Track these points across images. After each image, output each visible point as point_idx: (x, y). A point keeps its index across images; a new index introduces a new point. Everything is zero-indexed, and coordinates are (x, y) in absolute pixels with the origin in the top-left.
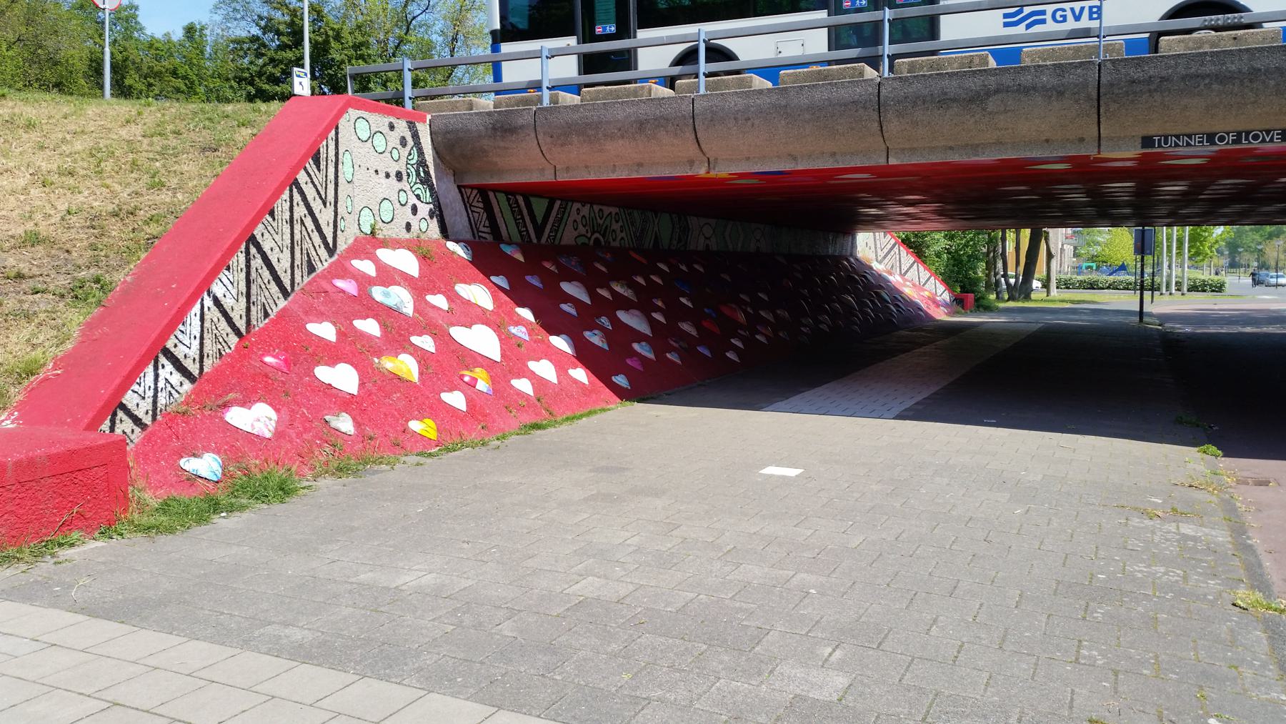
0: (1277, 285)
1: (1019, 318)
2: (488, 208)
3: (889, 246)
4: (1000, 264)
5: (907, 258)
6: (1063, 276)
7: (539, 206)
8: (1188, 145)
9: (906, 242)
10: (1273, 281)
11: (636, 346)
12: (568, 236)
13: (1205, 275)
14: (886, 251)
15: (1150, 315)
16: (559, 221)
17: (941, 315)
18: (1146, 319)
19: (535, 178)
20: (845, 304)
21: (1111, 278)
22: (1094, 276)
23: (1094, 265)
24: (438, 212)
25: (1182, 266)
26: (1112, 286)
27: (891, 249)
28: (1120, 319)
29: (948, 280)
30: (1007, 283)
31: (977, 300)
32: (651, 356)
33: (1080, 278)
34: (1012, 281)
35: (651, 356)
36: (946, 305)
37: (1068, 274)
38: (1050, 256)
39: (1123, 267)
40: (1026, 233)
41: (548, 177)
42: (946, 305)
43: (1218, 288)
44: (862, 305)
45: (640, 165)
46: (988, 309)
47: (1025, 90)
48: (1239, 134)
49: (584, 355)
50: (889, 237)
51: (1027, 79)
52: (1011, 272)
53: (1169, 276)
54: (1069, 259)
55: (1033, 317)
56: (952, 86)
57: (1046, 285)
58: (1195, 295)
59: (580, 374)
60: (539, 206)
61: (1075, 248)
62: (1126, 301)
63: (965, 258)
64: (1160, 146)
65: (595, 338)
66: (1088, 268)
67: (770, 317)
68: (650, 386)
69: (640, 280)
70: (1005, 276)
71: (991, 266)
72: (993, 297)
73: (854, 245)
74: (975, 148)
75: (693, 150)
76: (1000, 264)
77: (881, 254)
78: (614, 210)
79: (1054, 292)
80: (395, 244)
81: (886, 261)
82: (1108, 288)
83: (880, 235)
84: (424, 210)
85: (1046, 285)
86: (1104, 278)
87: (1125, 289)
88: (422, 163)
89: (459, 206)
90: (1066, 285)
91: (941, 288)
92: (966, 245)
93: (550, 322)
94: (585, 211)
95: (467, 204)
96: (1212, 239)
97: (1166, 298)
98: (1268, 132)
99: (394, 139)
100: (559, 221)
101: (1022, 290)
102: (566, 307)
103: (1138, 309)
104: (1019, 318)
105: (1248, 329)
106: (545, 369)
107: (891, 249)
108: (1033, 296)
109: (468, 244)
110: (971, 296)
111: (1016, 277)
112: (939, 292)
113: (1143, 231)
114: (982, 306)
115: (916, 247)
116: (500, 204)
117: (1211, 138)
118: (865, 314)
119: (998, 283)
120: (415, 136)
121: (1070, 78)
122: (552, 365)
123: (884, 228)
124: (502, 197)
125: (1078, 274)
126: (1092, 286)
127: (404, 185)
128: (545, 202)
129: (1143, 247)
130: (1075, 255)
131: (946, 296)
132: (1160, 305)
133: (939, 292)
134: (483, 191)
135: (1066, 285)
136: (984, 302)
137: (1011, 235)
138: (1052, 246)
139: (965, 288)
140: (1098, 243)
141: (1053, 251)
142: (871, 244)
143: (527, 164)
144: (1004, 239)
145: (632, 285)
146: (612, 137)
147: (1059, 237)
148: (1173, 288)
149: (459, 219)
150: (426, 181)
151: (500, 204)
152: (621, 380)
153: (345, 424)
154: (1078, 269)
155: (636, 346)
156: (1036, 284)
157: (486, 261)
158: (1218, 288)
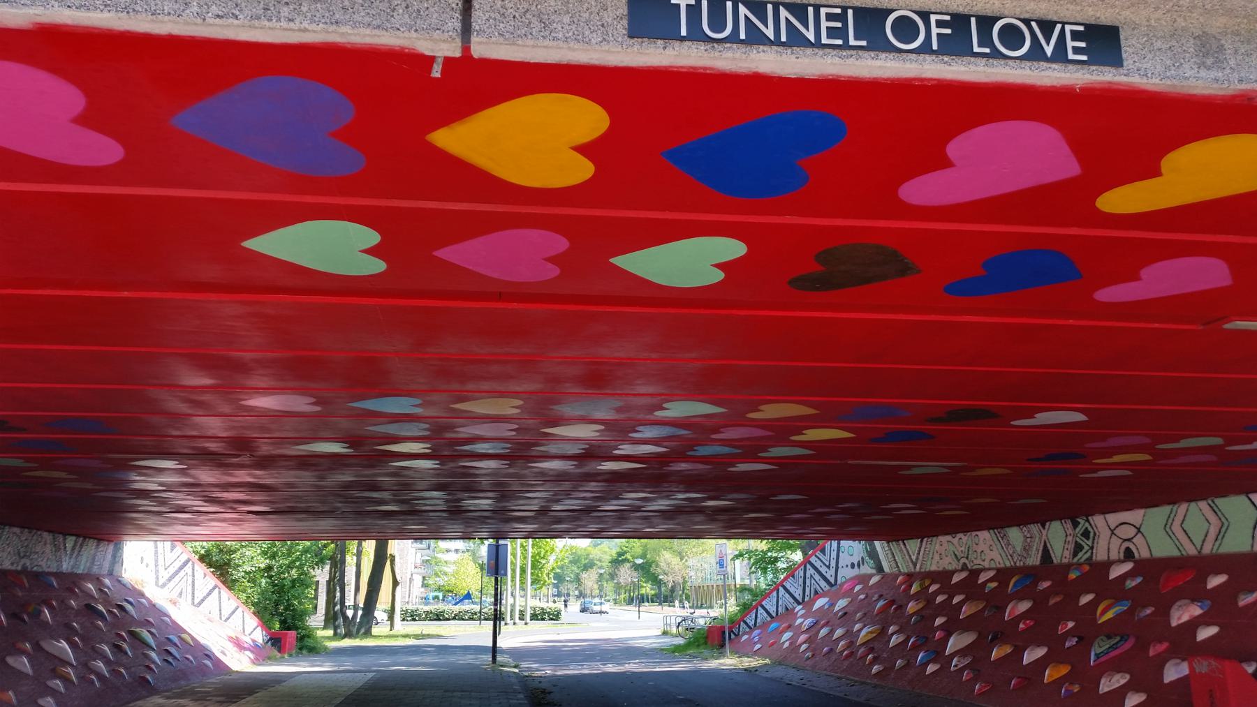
0: (601, 612)
3: (178, 564)
5: (205, 579)
6: (410, 607)
8: (796, 40)
9: (205, 558)
10: (597, 608)
14: (172, 570)
15: (503, 651)
17: (240, 663)
18: (499, 658)
21: (457, 608)
22: (441, 607)
23: (441, 595)
25: (525, 596)
26: (458, 617)
27: (181, 568)
28: (468, 659)
29: (263, 611)
31: (301, 639)
33: (427, 608)
37: (415, 605)
38: (395, 583)
39: (468, 596)
40: (370, 546)
42: (255, 648)
43: (555, 616)
48: (959, 21)
50: (179, 548)
52: (349, 602)
53: (513, 606)
54: (418, 590)
55: (366, 660)
62: (479, 634)
63: (287, 583)
64: (696, 35)
66: (436, 598)
73: (117, 558)
77: (164, 575)
79: (400, 627)
81: (172, 584)
82: (454, 618)
86: (449, 608)
87: (471, 619)
90: (412, 616)
91: (252, 622)
92: (290, 567)
96: (549, 566)
98: (1047, 27)
103: (490, 644)
105: (611, 668)
107: (181, 568)
110: (293, 633)
112: (248, 630)
113: (497, 547)
115: (220, 565)
123: (151, 532)
125: (427, 604)
126: (438, 617)
129: (496, 567)
130: (424, 585)
131: (259, 636)
132: (514, 637)
133: (248, 630)
135: (412, 616)
136: (309, 642)
138: (397, 571)
139: (283, 619)
140: (445, 574)
141: (398, 578)
142: (150, 559)
147: (405, 552)
148: (517, 616)
154: (425, 600)
156: (380, 614)
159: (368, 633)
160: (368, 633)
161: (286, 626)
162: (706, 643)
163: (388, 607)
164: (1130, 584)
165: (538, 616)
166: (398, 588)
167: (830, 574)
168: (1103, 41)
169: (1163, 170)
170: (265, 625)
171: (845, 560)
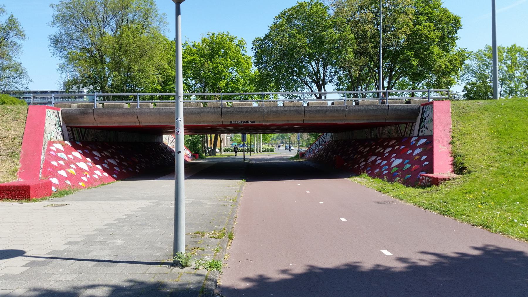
1: (211, 161)
2: (72, 132)
4: (206, 145)
7: (83, 130)
11: (115, 168)
12: (90, 139)
13: (267, 147)
16: (87, 134)
19: (91, 125)
20: (163, 157)
24: (63, 134)
28: (239, 160)
30: (208, 151)
31: (199, 156)
32: (119, 170)
34: (210, 150)
35: (119, 170)
36: (190, 157)
38: (221, 141)
40: (213, 136)
41: (95, 125)
42: (190, 157)
43: (272, 151)
44: (167, 157)
45: (121, 123)
46: (203, 158)
47: (208, 112)
49: (105, 170)
51: (208, 110)
52: (209, 147)
56: (194, 110)
57: (220, 151)
58: (265, 153)
59: (106, 174)
60: (83, 130)
61: (231, 138)
65: (106, 166)
67: (144, 161)
68: (121, 177)
69: (110, 151)
70: (208, 148)
71: (203, 145)
72: (204, 155)
73: (162, 139)
74: (199, 122)
75: (136, 120)
76: (206, 145)
77: (170, 142)
78: (100, 131)
79: (223, 153)
80: (56, 142)
83: (170, 136)
84: (60, 133)
85: (220, 151)
88: (59, 121)
89: (67, 132)
90: (227, 151)
91: (189, 152)
92: (195, 139)
93: (96, 162)
94: (93, 131)
95: (68, 131)
97: (256, 154)
99: (54, 115)
100: (87, 134)
101: (213, 153)
102: (96, 158)
104: (211, 161)
106: (98, 172)
108: (216, 154)
109: (70, 142)
111: (211, 148)
114: (201, 158)
116: (75, 131)
117: (242, 122)
118: (169, 160)
119: (205, 150)
120: (58, 114)
121: (216, 110)
122: (99, 172)
124: (75, 129)
127: (56, 127)
128: (84, 129)
129: (244, 139)
131: (190, 155)
134: (71, 127)
135: (227, 151)
137: (209, 136)
143: (89, 121)
144: (207, 137)
145: (109, 152)
146: (115, 116)
149: (66, 136)
150: (60, 126)
151: (75, 131)
152: (114, 176)
153: (68, 182)
155: (115, 168)
156: (217, 150)
157: (76, 147)
158: (272, 151)
159: (215, 155)
160: (215, 155)
161: (195, 153)
162: (464, 168)
163: (219, 148)
164: (96, 158)
165: (265, 151)
166: (222, 143)
167: (324, 140)
168: (254, 122)
169: (454, 11)
170: (191, 152)
171: (328, 137)
